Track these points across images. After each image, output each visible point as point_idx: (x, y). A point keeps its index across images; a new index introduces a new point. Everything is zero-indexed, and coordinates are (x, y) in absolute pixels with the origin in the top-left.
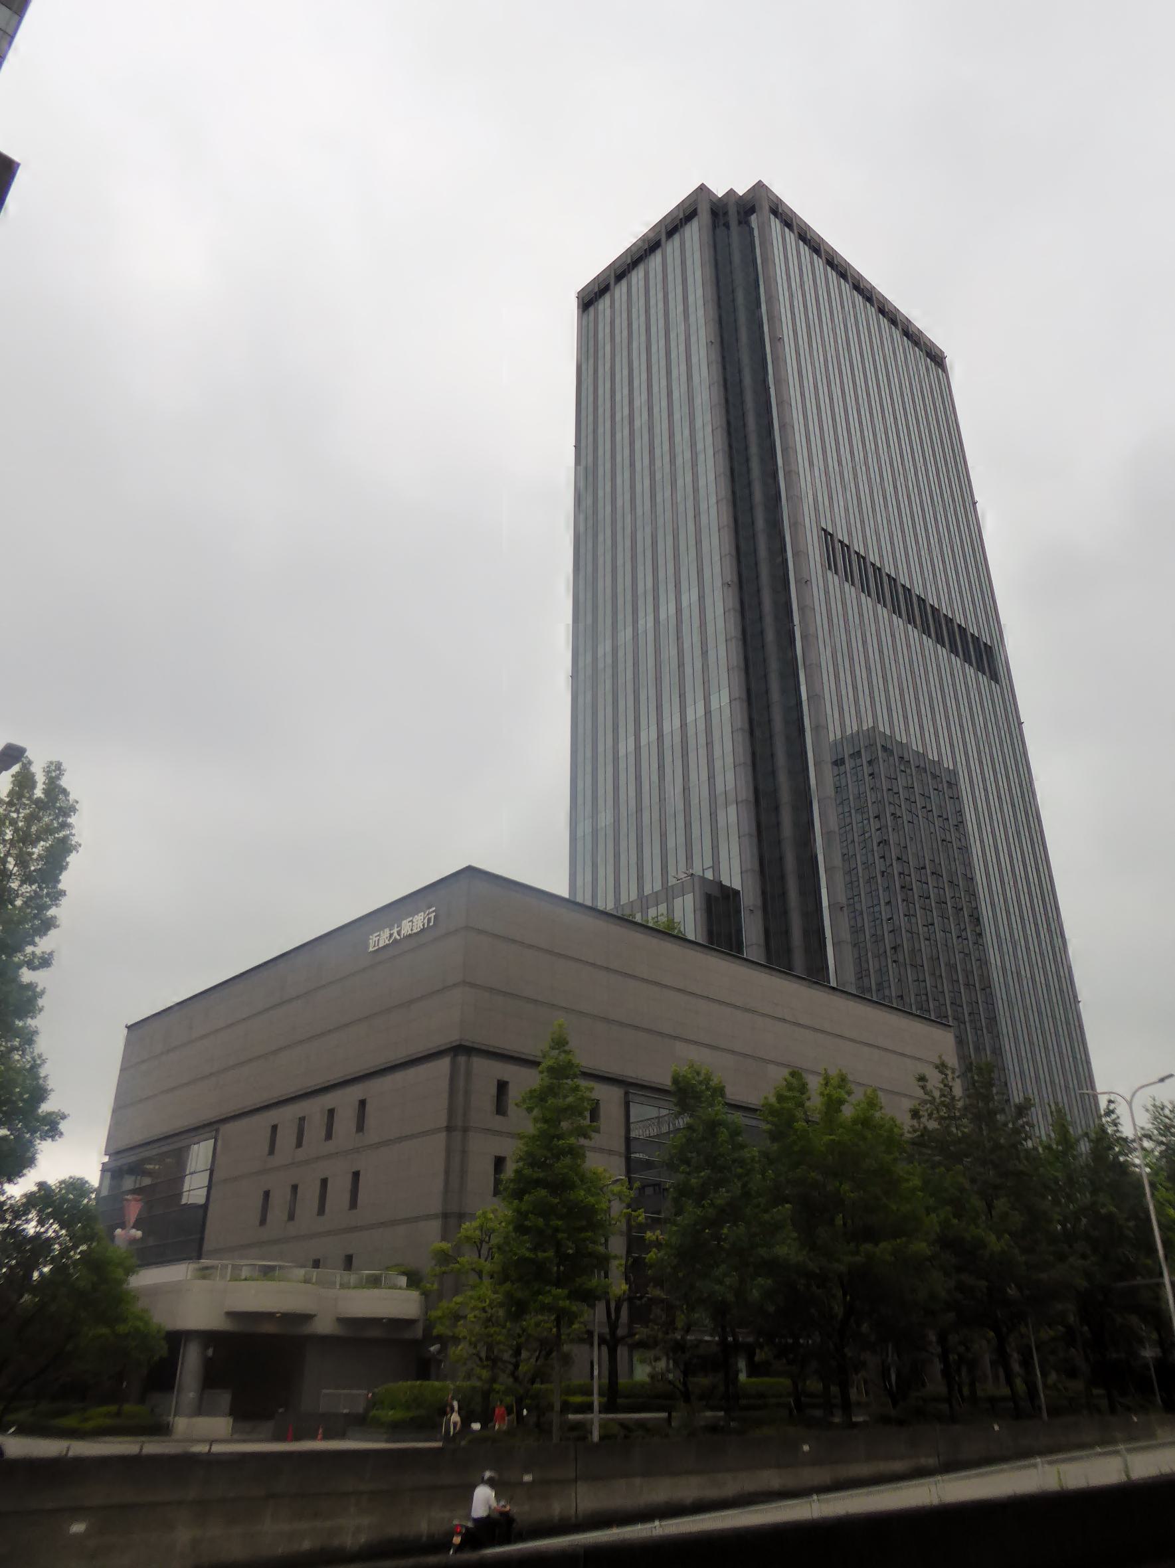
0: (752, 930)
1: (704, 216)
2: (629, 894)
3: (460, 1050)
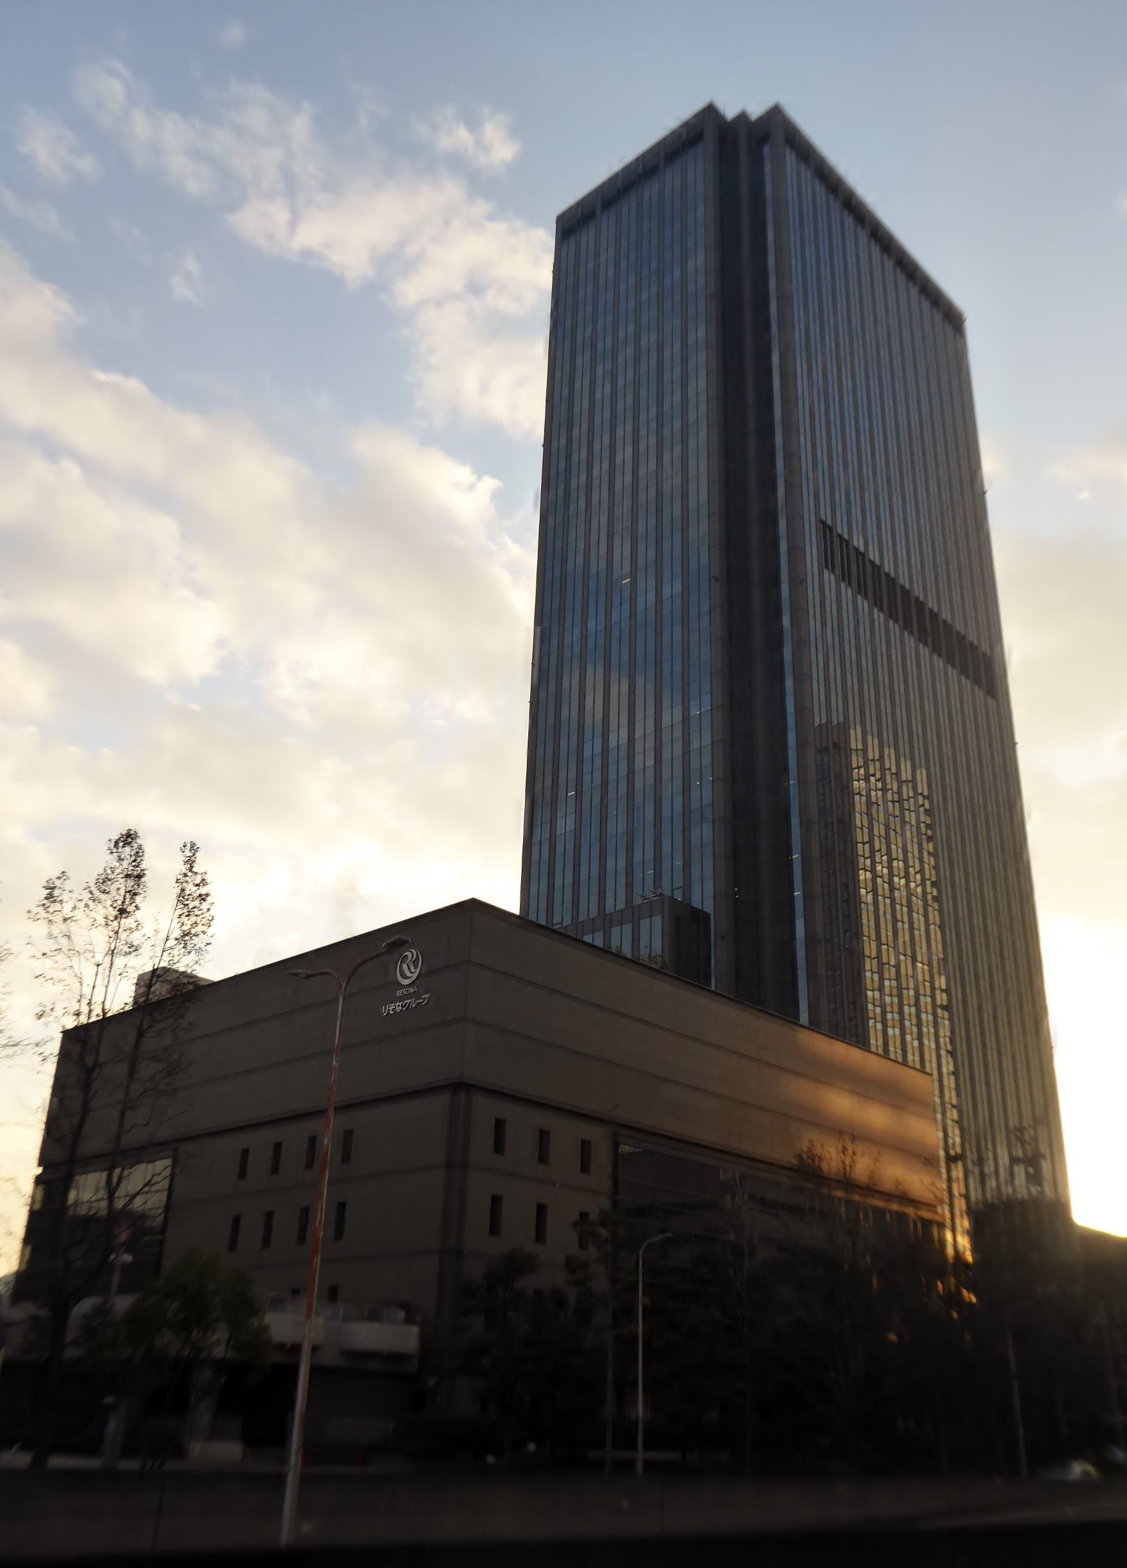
0: (720, 956)
1: (709, 144)
2: (589, 908)
3: (460, 1087)
